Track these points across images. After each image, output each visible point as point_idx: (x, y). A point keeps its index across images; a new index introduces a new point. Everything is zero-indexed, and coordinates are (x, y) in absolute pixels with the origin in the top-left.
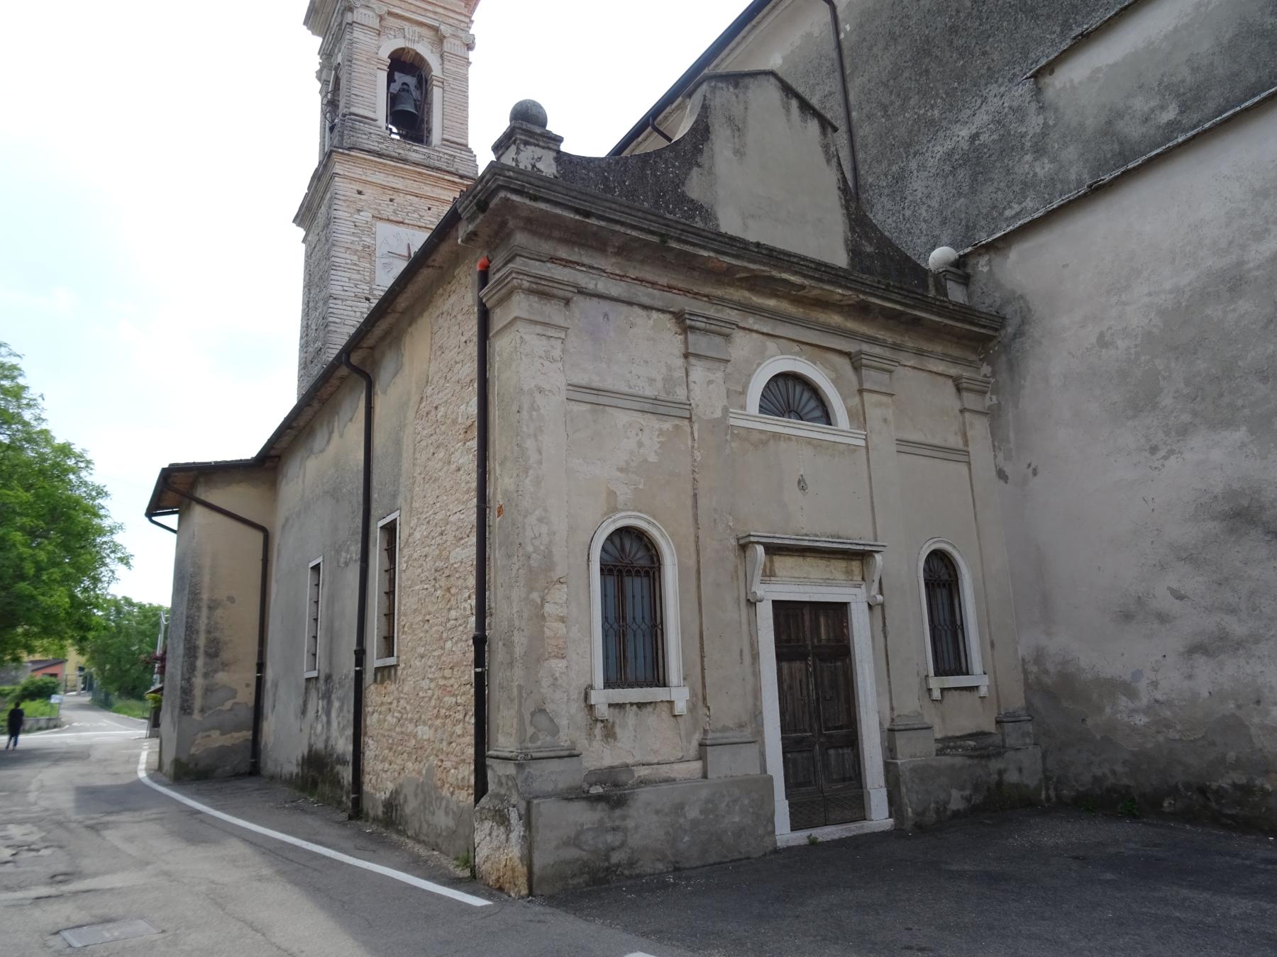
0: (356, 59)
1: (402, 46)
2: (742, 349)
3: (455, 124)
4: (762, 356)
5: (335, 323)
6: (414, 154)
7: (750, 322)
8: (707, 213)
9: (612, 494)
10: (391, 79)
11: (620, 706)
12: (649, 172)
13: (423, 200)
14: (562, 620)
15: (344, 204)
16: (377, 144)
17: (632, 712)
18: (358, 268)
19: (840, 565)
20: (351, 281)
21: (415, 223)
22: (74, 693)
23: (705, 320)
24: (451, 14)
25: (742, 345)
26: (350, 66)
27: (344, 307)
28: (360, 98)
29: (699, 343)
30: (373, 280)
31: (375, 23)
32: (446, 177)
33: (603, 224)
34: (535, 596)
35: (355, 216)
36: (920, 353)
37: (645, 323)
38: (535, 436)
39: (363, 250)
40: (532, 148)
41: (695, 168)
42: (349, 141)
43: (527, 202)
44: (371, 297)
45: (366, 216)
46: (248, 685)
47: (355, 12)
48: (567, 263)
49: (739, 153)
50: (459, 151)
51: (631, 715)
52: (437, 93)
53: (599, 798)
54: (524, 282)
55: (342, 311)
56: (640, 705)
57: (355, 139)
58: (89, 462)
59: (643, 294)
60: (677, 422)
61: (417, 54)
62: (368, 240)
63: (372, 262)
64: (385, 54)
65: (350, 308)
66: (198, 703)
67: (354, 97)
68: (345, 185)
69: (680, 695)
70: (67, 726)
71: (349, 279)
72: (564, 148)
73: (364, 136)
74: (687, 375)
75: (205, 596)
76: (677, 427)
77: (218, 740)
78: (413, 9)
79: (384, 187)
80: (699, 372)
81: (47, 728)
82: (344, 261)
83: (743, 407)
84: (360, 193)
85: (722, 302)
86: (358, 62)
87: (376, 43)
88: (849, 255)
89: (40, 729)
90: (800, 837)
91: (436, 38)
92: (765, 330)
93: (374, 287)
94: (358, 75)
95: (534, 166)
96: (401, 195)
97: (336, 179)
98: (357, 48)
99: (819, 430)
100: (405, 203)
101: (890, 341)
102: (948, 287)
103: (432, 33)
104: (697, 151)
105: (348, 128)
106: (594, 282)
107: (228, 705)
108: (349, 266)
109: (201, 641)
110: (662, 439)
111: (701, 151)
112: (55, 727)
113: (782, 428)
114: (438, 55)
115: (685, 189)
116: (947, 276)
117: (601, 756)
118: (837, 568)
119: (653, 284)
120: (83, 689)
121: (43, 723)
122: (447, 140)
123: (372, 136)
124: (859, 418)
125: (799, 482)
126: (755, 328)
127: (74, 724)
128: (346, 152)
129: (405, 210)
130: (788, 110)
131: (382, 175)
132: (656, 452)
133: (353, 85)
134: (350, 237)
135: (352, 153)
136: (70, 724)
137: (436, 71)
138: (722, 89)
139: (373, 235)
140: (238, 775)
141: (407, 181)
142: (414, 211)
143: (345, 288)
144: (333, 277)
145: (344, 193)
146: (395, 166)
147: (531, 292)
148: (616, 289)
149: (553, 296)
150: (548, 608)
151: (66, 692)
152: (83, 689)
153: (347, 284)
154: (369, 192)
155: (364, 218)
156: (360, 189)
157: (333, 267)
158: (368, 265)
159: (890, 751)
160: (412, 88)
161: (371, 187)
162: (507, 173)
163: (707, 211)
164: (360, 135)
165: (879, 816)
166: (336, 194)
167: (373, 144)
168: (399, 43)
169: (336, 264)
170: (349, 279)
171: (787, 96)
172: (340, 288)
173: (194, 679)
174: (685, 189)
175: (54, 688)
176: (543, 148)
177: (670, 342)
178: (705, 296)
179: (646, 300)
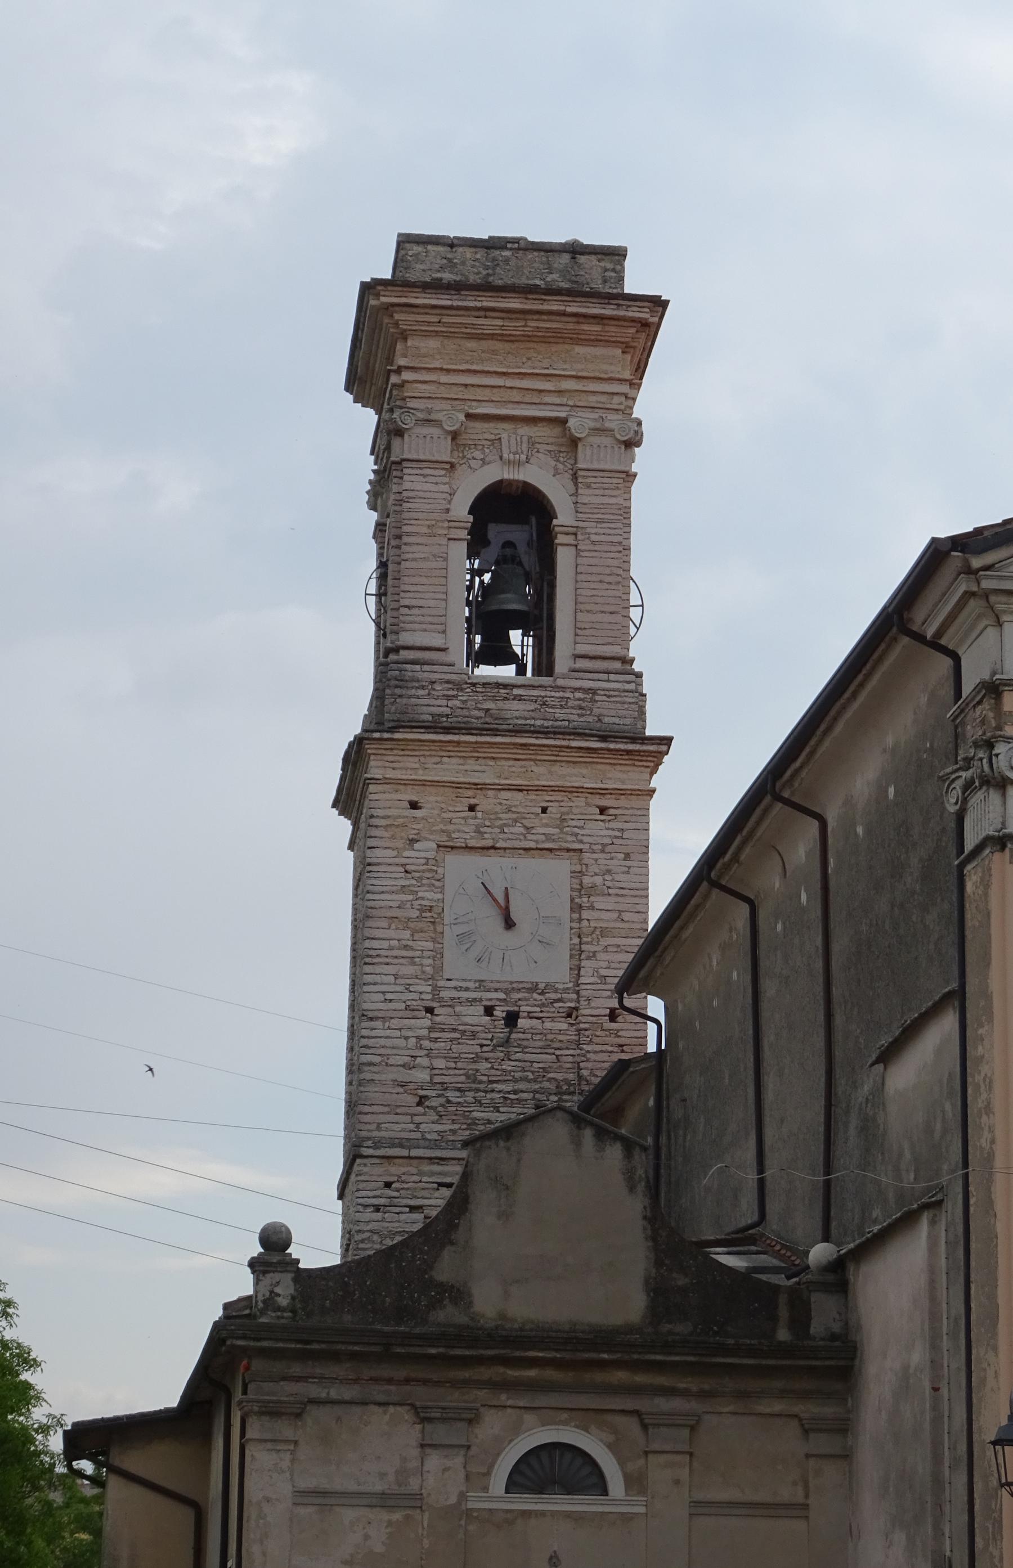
0: (409, 534)
2: (492, 1428)
3: (600, 617)
4: (516, 1430)
5: (371, 1064)
6: (515, 705)
10: (477, 544)
12: (393, 1265)
13: (532, 796)
15: (386, 834)
16: (444, 702)
18: (410, 954)
20: (399, 981)
23: (440, 1410)
24: (592, 386)
25: (492, 1424)
26: (399, 547)
27: (388, 1033)
29: (440, 1433)
30: (439, 969)
31: (443, 451)
32: (574, 744)
33: (323, 1346)
35: (406, 854)
36: (742, 1395)
37: (379, 1419)
38: (262, 1543)
39: (420, 917)
40: (272, 1275)
42: (393, 708)
43: (252, 1343)
44: (434, 1004)
45: (427, 848)
47: (406, 436)
48: (298, 1379)
49: (505, 1215)
50: (605, 676)
52: (564, 558)
54: (255, 1407)
55: (382, 1042)
57: (405, 701)
59: (377, 1392)
60: (410, 1512)
61: (526, 484)
63: (437, 938)
64: (461, 509)
65: (398, 1033)
67: (405, 611)
68: (387, 796)
71: (396, 976)
73: (421, 692)
74: (422, 1465)
76: (407, 1517)
78: (516, 396)
79: (457, 786)
80: (434, 1461)
82: (385, 944)
83: (486, 1489)
84: (414, 805)
88: (648, 1295)
92: (521, 1404)
93: (441, 983)
94: (413, 564)
95: (272, 1292)
96: (491, 793)
97: (372, 788)
99: (567, 1501)
100: (498, 808)
102: (813, 1299)
103: (557, 430)
104: (452, 1227)
105: (393, 682)
106: (327, 1390)
108: (395, 953)
110: (389, 1530)
111: (457, 1225)
113: (534, 1504)
114: (568, 476)
115: (433, 1273)
116: (810, 1288)
119: (390, 1381)
123: (437, 687)
124: (635, 1482)
126: (508, 1404)
128: (386, 735)
130: (577, 1143)
131: (454, 760)
132: (383, 1542)
133: (403, 587)
134: (394, 897)
135: (397, 736)
137: (564, 517)
138: (490, 1147)
139: (437, 882)
142: (516, 821)
143: (389, 996)
145: (388, 812)
146: (476, 743)
147: (261, 1413)
148: (348, 1393)
149: (283, 1414)
154: (429, 799)
155: (423, 854)
156: (415, 798)
157: (367, 960)
158: (429, 945)
160: (522, 549)
161: (433, 790)
162: (229, 1328)
163: (458, 1290)
166: (372, 816)
167: (439, 702)
168: (491, 474)
169: (371, 952)
170: (396, 976)
171: (579, 1128)
172: (381, 997)
174: (433, 1273)
176: (281, 1272)
177: (409, 1434)
178: (449, 1382)
179: (381, 1398)
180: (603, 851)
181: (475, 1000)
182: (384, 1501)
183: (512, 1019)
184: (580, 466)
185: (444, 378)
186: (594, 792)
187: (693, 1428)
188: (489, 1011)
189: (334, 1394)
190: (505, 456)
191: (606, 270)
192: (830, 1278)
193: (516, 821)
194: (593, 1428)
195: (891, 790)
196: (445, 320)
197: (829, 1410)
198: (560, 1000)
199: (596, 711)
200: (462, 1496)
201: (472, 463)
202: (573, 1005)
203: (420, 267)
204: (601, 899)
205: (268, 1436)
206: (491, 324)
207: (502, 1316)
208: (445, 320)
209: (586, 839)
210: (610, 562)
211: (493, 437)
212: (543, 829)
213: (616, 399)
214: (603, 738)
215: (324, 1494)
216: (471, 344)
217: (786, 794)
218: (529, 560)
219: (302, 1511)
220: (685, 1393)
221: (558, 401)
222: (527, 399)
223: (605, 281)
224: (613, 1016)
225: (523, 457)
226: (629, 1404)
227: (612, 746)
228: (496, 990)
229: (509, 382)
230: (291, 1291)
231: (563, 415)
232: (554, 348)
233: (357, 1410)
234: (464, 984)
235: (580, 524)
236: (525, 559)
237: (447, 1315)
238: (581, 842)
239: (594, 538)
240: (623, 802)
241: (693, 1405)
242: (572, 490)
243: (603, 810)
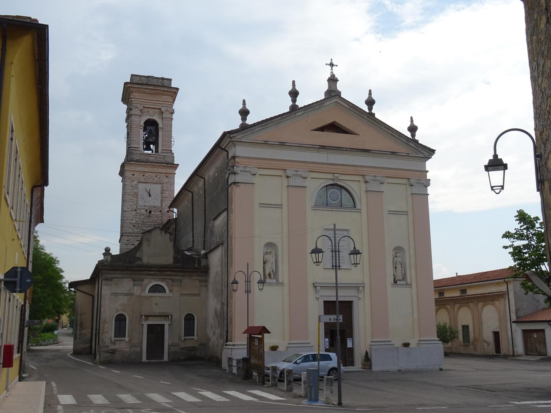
0: (133, 127)
1: (149, 118)
4: (150, 282)
6: (151, 158)
7: (148, 277)
8: (140, 259)
9: (117, 309)
11: (117, 340)
13: (154, 174)
14: (107, 328)
16: (139, 157)
17: (118, 341)
18: (132, 200)
19: (164, 318)
21: (151, 182)
22: (66, 328)
25: (146, 281)
27: (128, 214)
28: (134, 141)
30: (137, 203)
31: (139, 113)
32: (162, 165)
34: (103, 325)
35: (132, 183)
37: (126, 281)
41: (139, 251)
45: (135, 182)
46: (89, 333)
48: (111, 274)
51: (118, 342)
52: (160, 133)
53: (110, 352)
56: (120, 340)
57: (132, 157)
58: (58, 261)
59: (125, 276)
60: (131, 296)
61: (153, 119)
62: (136, 190)
63: (137, 198)
64: (142, 123)
65: (130, 214)
66: (78, 337)
69: (127, 339)
70: (61, 343)
71: (130, 204)
72: (112, 254)
73: (135, 155)
75: (79, 312)
77: (82, 346)
78: (152, 104)
79: (141, 172)
80: (136, 288)
81: (53, 344)
82: (128, 199)
84: (133, 175)
85: (142, 274)
86: (133, 124)
87: (139, 119)
89: (50, 344)
90: (148, 361)
91: (160, 112)
92: (151, 278)
96: (147, 173)
98: (133, 123)
101: (181, 275)
103: (159, 110)
107: (85, 338)
109: (79, 323)
112: (56, 343)
114: (161, 118)
117: (112, 347)
118: (163, 318)
119: (128, 274)
120: (70, 327)
121: (51, 342)
122: (163, 150)
124: (171, 291)
125: (156, 304)
127: (63, 343)
128: (128, 162)
129: (148, 178)
130: (161, 234)
136: (62, 342)
137: (160, 125)
139: (137, 188)
140: (87, 354)
141: (149, 168)
142: (151, 178)
143: (128, 208)
144: (125, 205)
147: (104, 280)
148: (120, 276)
150: (105, 327)
151: (63, 328)
152: (70, 327)
153: (129, 206)
154: (136, 174)
155: (135, 183)
156: (133, 174)
158: (136, 199)
159: (169, 349)
160: (153, 131)
164: (133, 155)
165: (166, 358)
170: (130, 204)
172: (127, 208)
173: (77, 332)
175: (56, 327)
177: (131, 283)
179: (126, 277)
180: (166, 183)
181: (144, 209)
182: (126, 294)
183: (150, 212)
184: (163, 117)
185: (139, 100)
186: (165, 173)
187: (181, 282)
188: (146, 211)
189: (118, 276)
190: (150, 114)
191: (168, 83)
192: (204, 256)
193: (151, 178)
194: (164, 282)
195: (216, 174)
196: (139, 90)
197: (204, 278)
198: (158, 209)
199: (166, 159)
200: (140, 294)
201: (144, 115)
202: (161, 210)
203: (135, 80)
204: (166, 192)
205: (106, 284)
206: (147, 91)
207: (148, 263)
208: (139, 90)
209: (164, 181)
210: (168, 134)
211: (148, 111)
212: (156, 179)
213: (170, 105)
214: (167, 164)
215: (116, 293)
216: (144, 94)
217: (198, 174)
218: (154, 133)
219: (112, 297)
220: (180, 276)
221: (159, 105)
222: (154, 105)
223: (168, 85)
224: (168, 212)
225: (153, 115)
226: (170, 278)
227: (168, 165)
228: (148, 207)
229: (151, 101)
230: (110, 258)
231: (160, 108)
232: (159, 96)
233: (122, 279)
234: (142, 206)
235: (163, 127)
236: (153, 133)
237: (138, 263)
238: (163, 182)
239: (166, 129)
240: (170, 175)
241: (181, 278)
242: (162, 121)
243: (167, 176)
